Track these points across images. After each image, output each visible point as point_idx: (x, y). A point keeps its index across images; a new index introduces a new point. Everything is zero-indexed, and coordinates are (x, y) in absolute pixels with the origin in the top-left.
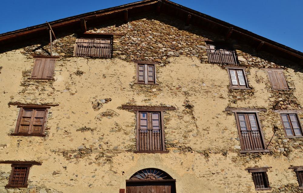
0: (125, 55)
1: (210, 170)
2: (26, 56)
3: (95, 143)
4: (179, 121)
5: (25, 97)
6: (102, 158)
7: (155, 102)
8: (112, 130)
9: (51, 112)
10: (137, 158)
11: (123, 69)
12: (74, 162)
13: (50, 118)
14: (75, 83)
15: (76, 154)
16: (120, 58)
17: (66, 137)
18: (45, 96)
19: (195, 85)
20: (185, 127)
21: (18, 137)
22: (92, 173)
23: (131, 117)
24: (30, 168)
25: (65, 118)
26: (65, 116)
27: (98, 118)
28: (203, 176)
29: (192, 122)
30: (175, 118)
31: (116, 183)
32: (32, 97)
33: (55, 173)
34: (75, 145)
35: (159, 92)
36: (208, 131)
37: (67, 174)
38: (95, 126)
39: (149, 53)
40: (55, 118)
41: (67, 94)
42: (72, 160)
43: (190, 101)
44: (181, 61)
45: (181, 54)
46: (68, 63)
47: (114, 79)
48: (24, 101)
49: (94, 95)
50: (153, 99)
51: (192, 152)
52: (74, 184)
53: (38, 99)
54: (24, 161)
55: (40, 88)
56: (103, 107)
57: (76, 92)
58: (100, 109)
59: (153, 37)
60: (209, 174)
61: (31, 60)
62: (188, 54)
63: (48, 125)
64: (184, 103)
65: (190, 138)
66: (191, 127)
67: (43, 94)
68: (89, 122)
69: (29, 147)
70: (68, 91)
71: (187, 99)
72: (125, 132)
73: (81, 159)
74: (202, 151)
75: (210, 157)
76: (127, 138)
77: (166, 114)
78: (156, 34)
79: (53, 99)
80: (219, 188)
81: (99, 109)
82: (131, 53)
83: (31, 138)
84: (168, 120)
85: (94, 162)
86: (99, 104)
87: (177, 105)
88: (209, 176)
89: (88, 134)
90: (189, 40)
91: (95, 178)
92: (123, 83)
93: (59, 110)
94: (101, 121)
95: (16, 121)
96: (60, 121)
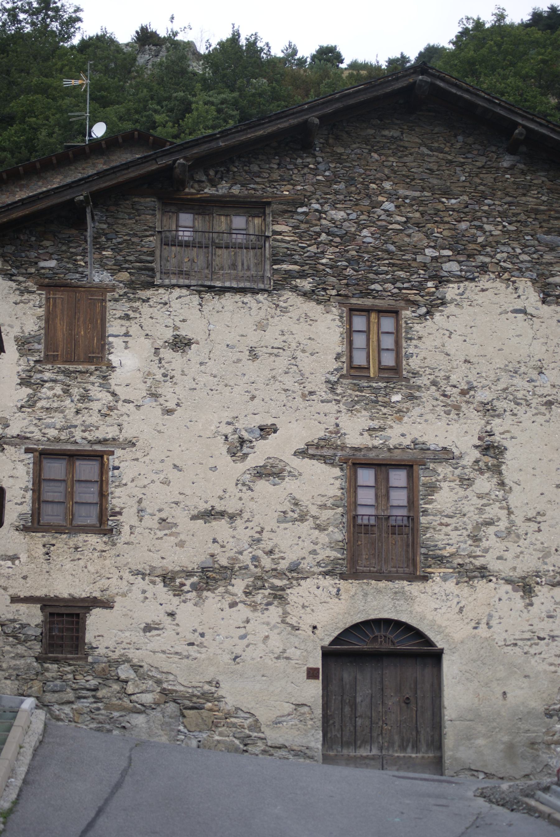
0: (310, 280)
1: (535, 628)
2: (14, 285)
3: (241, 553)
4: (461, 493)
5: (40, 419)
6: (260, 591)
7: (400, 434)
8: (284, 518)
9: (116, 464)
10: (347, 591)
11: (306, 326)
12: (193, 601)
13: (117, 484)
14: (173, 377)
15: (195, 579)
16: (295, 289)
17: (165, 537)
18: (95, 419)
19: (517, 381)
20: (476, 512)
21: (43, 536)
22: (239, 628)
23: (332, 481)
24: (87, 615)
25: (158, 483)
26: (155, 477)
27: (244, 484)
28: (515, 642)
29: (497, 496)
30: (452, 484)
31: (298, 652)
32: (58, 420)
33: (148, 628)
34: (190, 557)
35: (409, 404)
36: (539, 523)
37: (179, 630)
38: (239, 506)
39: (383, 268)
40: (129, 483)
41: (152, 411)
42: (189, 596)
43: (497, 433)
44: (480, 298)
45: (484, 268)
46: (145, 309)
47: (282, 362)
48: (39, 433)
49: (227, 415)
50: (391, 427)
51: (490, 581)
52: (199, 655)
53: (76, 427)
54: (66, 596)
55: (76, 392)
56: (255, 449)
57: (178, 405)
58: (249, 458)
59: (397, 207)
60: (529, 639)
61: (32, 297)
62: (505, 270)
63: (117, 504)
64: (480, 438)
65: (488, 542)
66: (493, 511)
67: (86, 411)
68: (221, 493)
69: (76, 563)
70: (156, 401)
71: (488, 428)
72: (318, 522)
73: (208, 594)
74: (516, 579)
75: (537, 596)
76: (323, 538)
77: (427, 473)
78: (407, 193)
79: (116, 428)
80: (553, 675)
81: (246, 455)
82: (327, 269)
83: (76, 539)
84: (433, 488)
85: (241, 602)
86: (242, 442)
87: (458, 444)
88: (529, 643)
89: (221, 527)
90: (514, 215)
91: (245, 642)
92: (307, 375)
93: (137, 459)
94: (252, 490)
95: (30, 493)
96: (143, 491)
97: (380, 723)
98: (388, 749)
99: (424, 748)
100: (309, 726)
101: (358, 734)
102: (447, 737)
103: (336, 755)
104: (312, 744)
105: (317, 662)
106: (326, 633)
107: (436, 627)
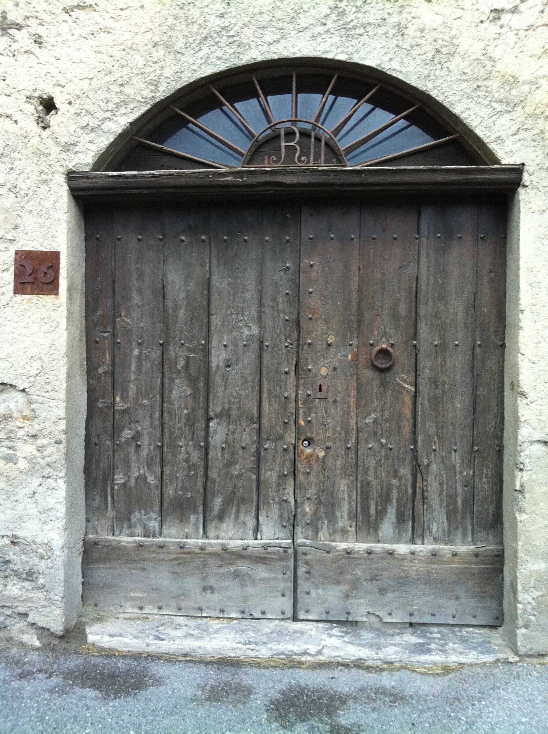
97: (290, 437)
98: (314, 526)
99: (438, 521)
100: (22, 464)
101: (213, 474)
102: (526, 502)
103: (141, 546)
104: (30, 530)
105: (55, 228)
106: (85, 120)
107: (494, 84)
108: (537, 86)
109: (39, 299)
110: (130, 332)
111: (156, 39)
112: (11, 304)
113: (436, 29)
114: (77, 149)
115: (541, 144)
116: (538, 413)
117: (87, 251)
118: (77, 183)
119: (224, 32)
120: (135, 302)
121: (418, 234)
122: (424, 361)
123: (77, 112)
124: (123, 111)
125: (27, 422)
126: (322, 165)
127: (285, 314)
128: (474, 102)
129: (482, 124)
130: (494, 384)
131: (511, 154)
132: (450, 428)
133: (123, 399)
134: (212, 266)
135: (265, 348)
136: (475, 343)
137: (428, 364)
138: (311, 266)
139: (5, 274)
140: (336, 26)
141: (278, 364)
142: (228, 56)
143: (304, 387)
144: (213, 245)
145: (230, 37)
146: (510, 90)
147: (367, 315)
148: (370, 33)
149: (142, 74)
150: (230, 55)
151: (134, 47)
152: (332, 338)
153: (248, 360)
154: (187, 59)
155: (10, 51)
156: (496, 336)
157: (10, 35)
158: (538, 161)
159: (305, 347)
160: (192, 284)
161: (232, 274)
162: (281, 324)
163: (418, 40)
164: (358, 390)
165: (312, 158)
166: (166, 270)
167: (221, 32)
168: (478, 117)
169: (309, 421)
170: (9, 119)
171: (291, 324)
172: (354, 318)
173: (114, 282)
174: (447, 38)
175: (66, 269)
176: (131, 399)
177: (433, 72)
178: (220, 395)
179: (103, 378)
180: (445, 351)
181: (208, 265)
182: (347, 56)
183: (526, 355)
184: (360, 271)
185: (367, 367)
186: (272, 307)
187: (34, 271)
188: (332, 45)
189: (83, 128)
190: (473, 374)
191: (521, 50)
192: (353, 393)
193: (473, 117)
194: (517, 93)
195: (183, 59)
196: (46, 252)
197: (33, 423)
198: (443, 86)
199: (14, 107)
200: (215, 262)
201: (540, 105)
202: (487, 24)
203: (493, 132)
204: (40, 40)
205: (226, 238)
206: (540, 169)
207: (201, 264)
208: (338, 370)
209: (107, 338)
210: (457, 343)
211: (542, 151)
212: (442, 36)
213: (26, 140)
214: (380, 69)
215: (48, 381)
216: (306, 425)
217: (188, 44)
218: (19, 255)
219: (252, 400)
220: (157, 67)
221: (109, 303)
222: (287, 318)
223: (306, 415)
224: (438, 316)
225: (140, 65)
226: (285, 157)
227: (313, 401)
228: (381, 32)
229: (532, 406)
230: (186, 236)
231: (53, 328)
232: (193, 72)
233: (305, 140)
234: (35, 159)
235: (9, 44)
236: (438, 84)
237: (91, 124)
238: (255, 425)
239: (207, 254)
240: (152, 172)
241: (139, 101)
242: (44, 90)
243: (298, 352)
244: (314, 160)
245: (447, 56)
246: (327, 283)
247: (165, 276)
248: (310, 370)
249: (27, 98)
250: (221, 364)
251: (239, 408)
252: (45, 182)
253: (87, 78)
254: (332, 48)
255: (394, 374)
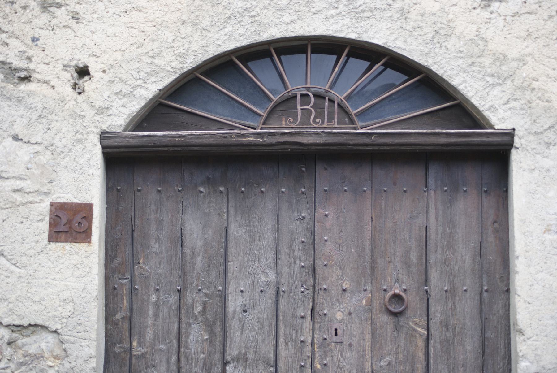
106: (117, 87)
107: (486, 61)
108: (524, 62)
109: (72, 246)
110: (147, 278)
111: (184, 17)
112: (45, 251)
113: (435, 14)
114: (110, 112)
115: (529, 112)
116: (534, 348)
117: (107, 202)
118: (108, 142)
119: (246, 13)
120: (154, 250)
121: (426, 187)
122: (436, 305)
123: (111, 79)
124: (153, 79)
125: (57, 361)
126: (336, 126)
127: (301, 261)
128: (470, 76)
129: (477, 95)
130: (501, 327)
131: (503, 121)
132: (461, 369)
133: (140, 344)
134: (229, 216)
135: (282, 293)
136: (482, 288)
137: (439, 308)
138: (326, 216)
139: (40, 224)
140: (347, 9)
141: (294, 309)
142: (249, 33)
143: (320, 331)
144: (230, 196)
145: (252, 17)
146: (500, 66)
147: (380, 262)
148: (376, 17)
149: (171, 47)
150: (251, 32)
151: (164, 24)
152: (346, 284)
153: (265, 305)
154: (212, 35)
155: (50, 26)
156: (502, 281)
157: (50, 12)
158: (526, 126)
159: (321, 293)
160: (210, 233)
161: (249, 223)
162: (297, 270)
163: (419, 23)
164: (373, 333)
165: (326, 120)
166: (184, 219)
167: (243, 12)
168: (474, 89)
169: (325, 365)
170: (46, 85)
171: (307, 271)
172: (367, 265)
173: (133, 231)
174: (445, 22)
175: (98, 219)
176: (148, 344)
177: (433, 50)
178: (237, 339)
179: (120, 323)
180: (455, 296)
181: (225, 215)
182: (357, 36)
183: (522, 296)
184: (372, 220)
185: (381, 311)
186: (288, 254)
187: (69, 222)
188: (343, 25)
189: (116, 94)
190: (481, 317)
191: (509, 32)
192: (368, 337)
193: (469, 88)
194: (507, 69)
195: (209, 35)
196: (80, 205)
197: (64, 362)
198: (442, 62)
199: (52, 74)
200: (232, 211)
201: (527, 79)
202: (478, 10)
203: (487, 101)
204: (77, 16)
205: (243, 189)
206: (529, 133)
207: (219, 214)
208: (353, 315)
209: (125, 284)
210: (465, 288)
211: (530, 118)
212: (440, 20)
213: (63, 104)
214: (387, 47)
215: (79, 322)
216: (322, 368)
217: (214, 23)
218: (54, 207)
219: (269, 343)
220: (185, 42)
221: (128, 251)
222: (303, 264)
223: (322, 359)
224: (447, 264)
225: (170, 40)
226: (301, 120)
227: (329, 345)
228: (386, 15)
229: (529, 342)
230: (205, 188)
231: (86, 273)
232: (217, 46)
233: (320, 101)
234: (71, 121)
235: (49, 20)
236: (438, 60)
237: (124, 90)
238: (272, 369)
239: (225, 205)
240: (180, 133)
241: (168, 71)
242: (80, 60)
243: (314, 298)
244: (328, 122)
245: (445, 37)
246: (341, 231)
247: (183, 225)
248: (325, 315)
249: (64, 66)
250: (238, 309)
251: (256, 352)
252: (80, 141)
253: (120, 50)
254: (343, 28)
255: (407, 318)
